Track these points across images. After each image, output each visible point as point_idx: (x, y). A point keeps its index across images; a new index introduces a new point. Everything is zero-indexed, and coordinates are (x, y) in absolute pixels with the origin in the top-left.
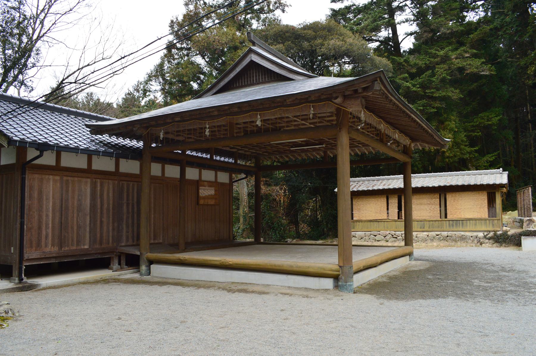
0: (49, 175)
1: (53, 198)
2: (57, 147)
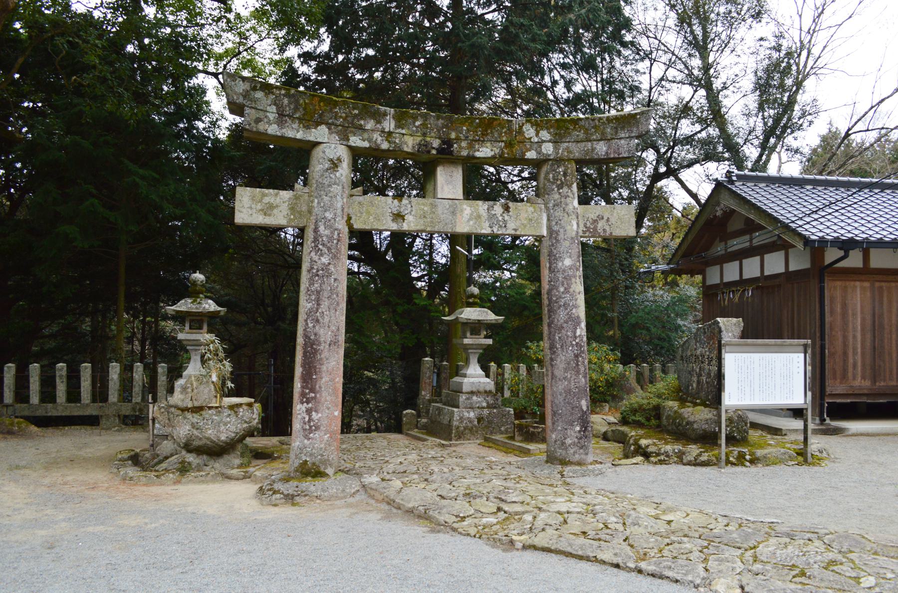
0: (855, 281)
1: (862, 313)
2: (867, 242)
